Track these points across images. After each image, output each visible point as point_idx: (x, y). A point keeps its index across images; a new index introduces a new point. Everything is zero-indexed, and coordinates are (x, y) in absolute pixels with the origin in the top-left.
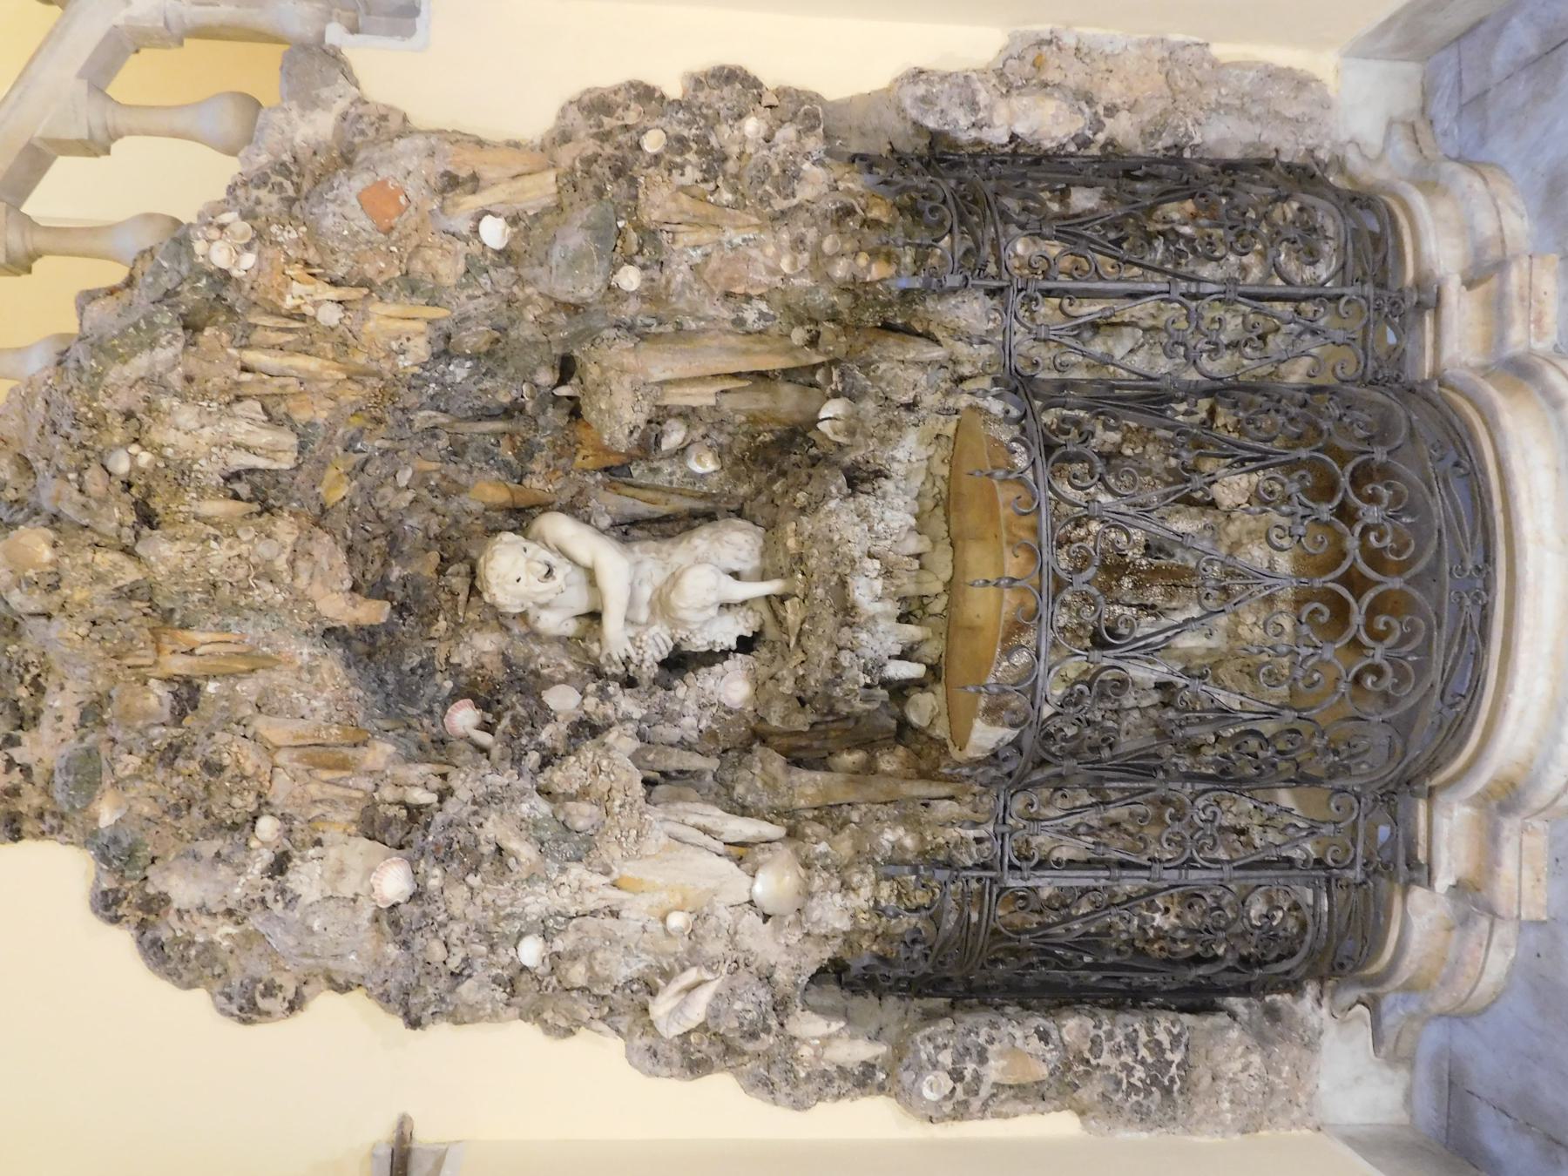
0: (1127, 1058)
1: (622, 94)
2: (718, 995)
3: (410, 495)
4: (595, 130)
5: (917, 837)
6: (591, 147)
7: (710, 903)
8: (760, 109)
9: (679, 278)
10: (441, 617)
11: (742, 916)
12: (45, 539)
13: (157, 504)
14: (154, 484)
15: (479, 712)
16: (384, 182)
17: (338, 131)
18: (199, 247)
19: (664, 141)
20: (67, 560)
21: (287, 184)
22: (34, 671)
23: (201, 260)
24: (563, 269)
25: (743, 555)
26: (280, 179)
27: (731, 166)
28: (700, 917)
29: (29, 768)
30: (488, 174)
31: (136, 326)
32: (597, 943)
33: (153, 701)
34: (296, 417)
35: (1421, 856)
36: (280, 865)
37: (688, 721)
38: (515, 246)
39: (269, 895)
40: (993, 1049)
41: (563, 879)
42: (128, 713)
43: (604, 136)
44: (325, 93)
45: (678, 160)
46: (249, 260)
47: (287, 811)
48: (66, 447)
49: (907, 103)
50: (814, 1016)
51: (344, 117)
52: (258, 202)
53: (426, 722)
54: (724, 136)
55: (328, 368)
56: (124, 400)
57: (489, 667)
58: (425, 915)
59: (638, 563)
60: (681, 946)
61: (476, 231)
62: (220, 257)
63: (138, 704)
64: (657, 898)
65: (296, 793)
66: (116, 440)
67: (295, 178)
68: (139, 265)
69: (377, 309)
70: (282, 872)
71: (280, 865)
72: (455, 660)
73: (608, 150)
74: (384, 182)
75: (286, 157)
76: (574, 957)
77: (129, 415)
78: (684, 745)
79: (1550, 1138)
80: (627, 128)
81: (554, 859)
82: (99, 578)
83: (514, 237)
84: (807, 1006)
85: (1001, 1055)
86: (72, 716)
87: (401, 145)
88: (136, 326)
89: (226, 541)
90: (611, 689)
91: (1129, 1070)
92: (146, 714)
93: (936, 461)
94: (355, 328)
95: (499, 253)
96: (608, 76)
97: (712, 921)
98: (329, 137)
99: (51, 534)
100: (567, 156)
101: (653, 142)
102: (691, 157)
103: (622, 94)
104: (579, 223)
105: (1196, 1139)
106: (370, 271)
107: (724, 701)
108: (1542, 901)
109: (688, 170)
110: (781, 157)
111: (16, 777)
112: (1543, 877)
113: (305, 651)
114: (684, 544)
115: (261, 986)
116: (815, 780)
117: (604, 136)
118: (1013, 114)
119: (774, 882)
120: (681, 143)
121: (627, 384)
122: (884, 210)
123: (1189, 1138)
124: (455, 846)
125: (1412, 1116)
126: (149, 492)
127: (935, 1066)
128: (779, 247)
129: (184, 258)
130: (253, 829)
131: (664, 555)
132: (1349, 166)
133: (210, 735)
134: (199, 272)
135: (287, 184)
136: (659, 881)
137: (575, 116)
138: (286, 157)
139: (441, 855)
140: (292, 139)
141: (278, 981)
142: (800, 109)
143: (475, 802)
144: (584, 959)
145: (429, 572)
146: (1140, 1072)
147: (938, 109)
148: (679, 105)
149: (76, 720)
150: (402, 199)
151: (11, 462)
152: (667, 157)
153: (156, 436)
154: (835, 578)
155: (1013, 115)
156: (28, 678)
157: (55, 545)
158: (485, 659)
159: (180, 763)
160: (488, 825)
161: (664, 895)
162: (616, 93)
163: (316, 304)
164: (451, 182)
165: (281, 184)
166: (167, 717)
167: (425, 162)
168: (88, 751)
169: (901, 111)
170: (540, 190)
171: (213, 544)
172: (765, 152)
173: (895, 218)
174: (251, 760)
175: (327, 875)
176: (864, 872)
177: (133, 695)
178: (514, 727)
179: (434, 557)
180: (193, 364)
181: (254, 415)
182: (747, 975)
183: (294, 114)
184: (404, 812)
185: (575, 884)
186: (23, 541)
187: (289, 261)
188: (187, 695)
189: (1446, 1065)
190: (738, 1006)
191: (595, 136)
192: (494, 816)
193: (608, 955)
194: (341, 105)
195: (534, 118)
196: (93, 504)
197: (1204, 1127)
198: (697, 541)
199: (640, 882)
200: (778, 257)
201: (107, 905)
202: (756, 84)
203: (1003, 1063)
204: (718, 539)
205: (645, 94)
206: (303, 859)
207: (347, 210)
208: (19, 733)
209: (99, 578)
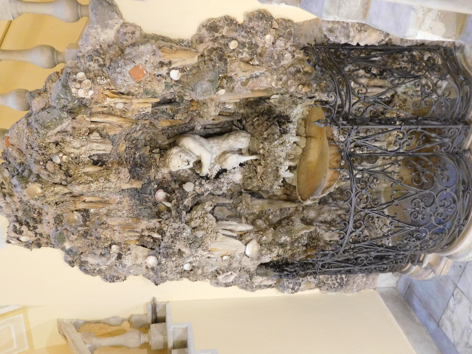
0: (334, 282)
1: (222, 22)
2: (236, 277)
3: (141, 132)
4: (212, 38)
5: (291, 238)
6: (211, 45)
7: (234, 253)
8: (272, 30)
9: (237, 86)
10: (153, 168)
11: (242, 257)
12: (38, 186)
13: (71, 172)
14: (69, 166)
15: (165, 193)
16: (138, 66)
17: (117, 38)
18: (73, 90)
19: (237, 45)
20: (47, 192)
21: (100, 59)
22: (38, 210)
23: (75, 95)
24: (201, 93)
25: (244, 145)
26: (97, 58)
27: (259, 51)
28: (231, 257)
29: (42, 234)
30: (173, 60)
31: (56, 119)
32: (204, 264)
33: (76, 217)
34: (110, 134)
35: (421, 259)
36: (120, 257)
37: (224, 188)
38: (182, 79)
39: (118, 264)
40: (302, 283)
41: (196, 254)
42: (69, 221)
43: (215, 40)
44: (110, 22)
45: (241, 51)
46: (91, 92)
47: (119, 242)
48: (37, 154)
49: (324, 29)
50: (259, 277)
51: (118, 31)
52: (90, 65)
53: (150, 197)
54: (258, 40)
55: (120, 121)
56: (54, 139)
57: (166, 177)
58: (161, 268)
59: (212, 147)
60: (226, 264)
61: (168, 74)
62: (81, 94)
63: (72, 218)
64: (220, 252)
65: (121, 237)
66: (54, 152)
67: (103, 57)
68: (48, 84)
69: (135, 101)
70: (120, 258)
71: (120, 257)
72: (157, 178)
73: (216, 45)
74: (138, 66)
75: (98, 47)
76: (198, 268)
77: (57, 144)
78: (224, 195)
79: (430, 314)
80: (223, 37)
81: (194, 249)
82: (57, 194)
83: (182, 76)
84: (257, 274)
85: (304, 284)
86: (52, 221)
87: (142, 48)
88: (56, 119)
89: (96, 183)
90: (203, 183)
91: (334, 284)
92: (75, 221)
93: (305, 111)
94: (128, 108)
95: (177, 81)
96: (217, 13)
97: (235, 259)
98: (113, 39)
99: (40, 185)
100: (201, 48)
101: (233, 45)
102: (246, 49)
103: (222, 22)
104: (207, 79)
105: (346, 294)
106: (132, 91)
107: (234, 181)
108: (447, 272)
109: (244, 54)
110: (278, 53)
111: (38, 236)
112: (449, 268)
113: (118, 197)
114: (226, 141)
115: (115, 278)
116: (259, 203)
117: (215, 40)
118: (361, 38)
119: (252, 248)
120: (242, 45)
121: (213, 105)
122: (310, 68)
123: (344, 294)
124: (169, 254)
125: (397, 286)
126: (68, 169)
127: (288, 287)
128: (272, 79)
129: (68, 95)
130: (111, 248)
131: (220, 144)
132: (465, 51)
133: (96, 230)
134: (74, 98)
135: (100, 59)
136: (221, 249)
137: (204, 31)
138: (98, 47)
139: (165, 256)
140: (99, 40)
141: (120, 276)
142: (286, 28)
143: (172, 237)
144: (201, 268)
145: (147, 153)
146: (337, 284)
147: (335, 35)
148: (241, 26)
149: (53, 222)
150: (145, 72)
151: (17, 151)
152: (237, 49)
153: (67, 150)
154: (275, 168)
155: (361, 39)
156: (36, 212)
157: (42, 188)
158: (165, 176)
159: (88, 237)
160: (176, 245)
161: (222, 252)
162: (219, 22)
163: (116, 104)
164: (162, 64)
165: (98, 59)
166: (82, 223)
167: (153, 57)
168: (60, 234)
169: (320, 30)
170: (191, 60)
171: (92, 184)
172: (272, 49)
173: (313, 71)
174: (108, 233)
175: (133, 258)
176: (276, 248)
177: (69, 215)
178: (177, 202)
179: (148, 148)
180: (75, 125)
181: (97, 138)
182: (244, 272)
183: (99, 30)
184: (152, 240)
185: (200, 256)
186: (31, 187)
187: (104, 89)
188: (85, 213)
189: (409, 283)
190: (241, 280)
191: (212, 40)
192: (178, 242)
193: (208, 267)
194: (117, 26)
195: (186, 29)
196: (51, 175)
197: (348, 291)
198: (230, 141)
199: (216, 249)
200: (272, 82)
201: (71, 263)
202: (271, 18)
203: (305, 286)
204: (236, 140)
205: (230, 21)
206: (125, 255)
207: (126, 79)
208: (36, 225)
209: (57, 194)
